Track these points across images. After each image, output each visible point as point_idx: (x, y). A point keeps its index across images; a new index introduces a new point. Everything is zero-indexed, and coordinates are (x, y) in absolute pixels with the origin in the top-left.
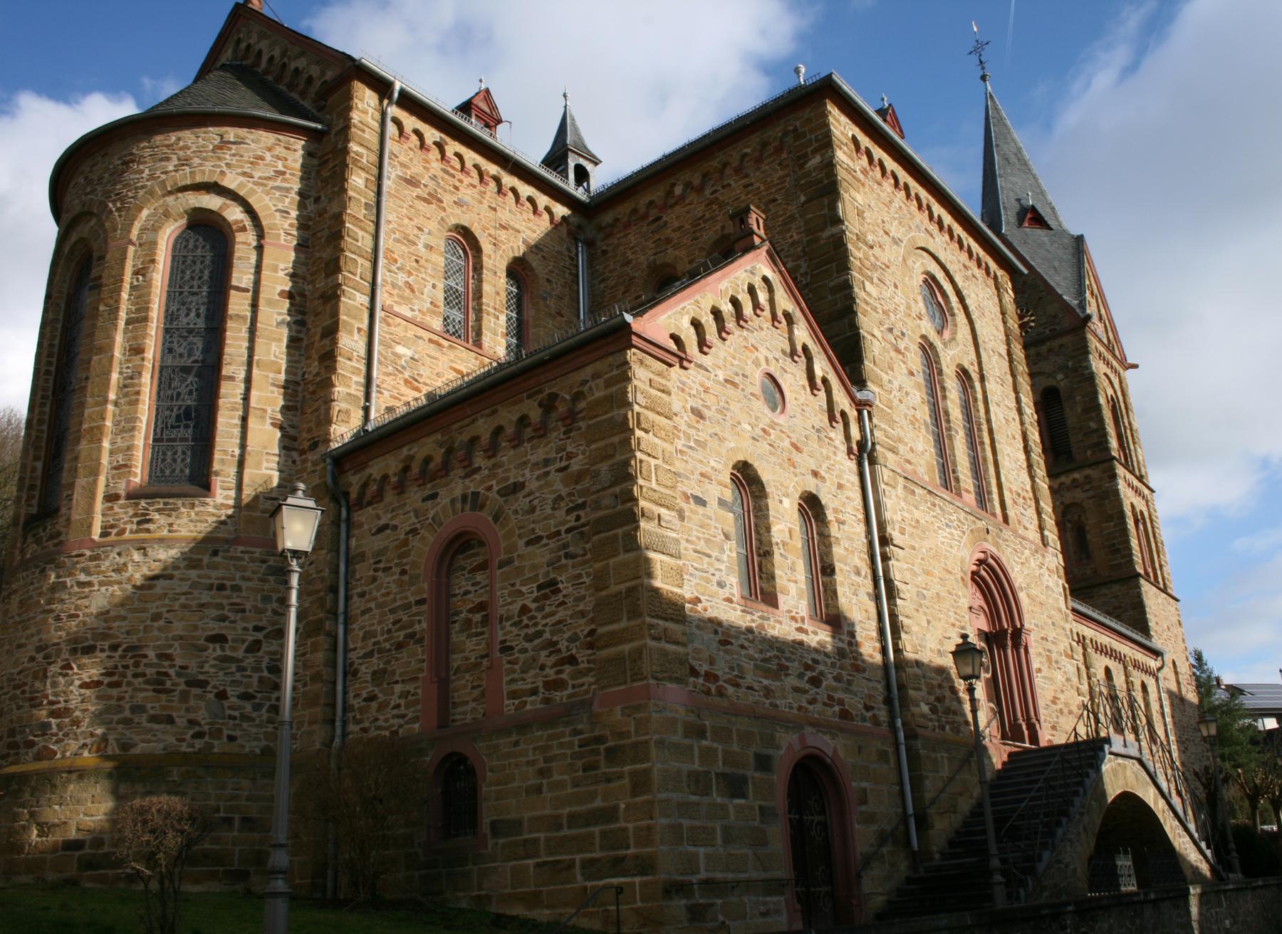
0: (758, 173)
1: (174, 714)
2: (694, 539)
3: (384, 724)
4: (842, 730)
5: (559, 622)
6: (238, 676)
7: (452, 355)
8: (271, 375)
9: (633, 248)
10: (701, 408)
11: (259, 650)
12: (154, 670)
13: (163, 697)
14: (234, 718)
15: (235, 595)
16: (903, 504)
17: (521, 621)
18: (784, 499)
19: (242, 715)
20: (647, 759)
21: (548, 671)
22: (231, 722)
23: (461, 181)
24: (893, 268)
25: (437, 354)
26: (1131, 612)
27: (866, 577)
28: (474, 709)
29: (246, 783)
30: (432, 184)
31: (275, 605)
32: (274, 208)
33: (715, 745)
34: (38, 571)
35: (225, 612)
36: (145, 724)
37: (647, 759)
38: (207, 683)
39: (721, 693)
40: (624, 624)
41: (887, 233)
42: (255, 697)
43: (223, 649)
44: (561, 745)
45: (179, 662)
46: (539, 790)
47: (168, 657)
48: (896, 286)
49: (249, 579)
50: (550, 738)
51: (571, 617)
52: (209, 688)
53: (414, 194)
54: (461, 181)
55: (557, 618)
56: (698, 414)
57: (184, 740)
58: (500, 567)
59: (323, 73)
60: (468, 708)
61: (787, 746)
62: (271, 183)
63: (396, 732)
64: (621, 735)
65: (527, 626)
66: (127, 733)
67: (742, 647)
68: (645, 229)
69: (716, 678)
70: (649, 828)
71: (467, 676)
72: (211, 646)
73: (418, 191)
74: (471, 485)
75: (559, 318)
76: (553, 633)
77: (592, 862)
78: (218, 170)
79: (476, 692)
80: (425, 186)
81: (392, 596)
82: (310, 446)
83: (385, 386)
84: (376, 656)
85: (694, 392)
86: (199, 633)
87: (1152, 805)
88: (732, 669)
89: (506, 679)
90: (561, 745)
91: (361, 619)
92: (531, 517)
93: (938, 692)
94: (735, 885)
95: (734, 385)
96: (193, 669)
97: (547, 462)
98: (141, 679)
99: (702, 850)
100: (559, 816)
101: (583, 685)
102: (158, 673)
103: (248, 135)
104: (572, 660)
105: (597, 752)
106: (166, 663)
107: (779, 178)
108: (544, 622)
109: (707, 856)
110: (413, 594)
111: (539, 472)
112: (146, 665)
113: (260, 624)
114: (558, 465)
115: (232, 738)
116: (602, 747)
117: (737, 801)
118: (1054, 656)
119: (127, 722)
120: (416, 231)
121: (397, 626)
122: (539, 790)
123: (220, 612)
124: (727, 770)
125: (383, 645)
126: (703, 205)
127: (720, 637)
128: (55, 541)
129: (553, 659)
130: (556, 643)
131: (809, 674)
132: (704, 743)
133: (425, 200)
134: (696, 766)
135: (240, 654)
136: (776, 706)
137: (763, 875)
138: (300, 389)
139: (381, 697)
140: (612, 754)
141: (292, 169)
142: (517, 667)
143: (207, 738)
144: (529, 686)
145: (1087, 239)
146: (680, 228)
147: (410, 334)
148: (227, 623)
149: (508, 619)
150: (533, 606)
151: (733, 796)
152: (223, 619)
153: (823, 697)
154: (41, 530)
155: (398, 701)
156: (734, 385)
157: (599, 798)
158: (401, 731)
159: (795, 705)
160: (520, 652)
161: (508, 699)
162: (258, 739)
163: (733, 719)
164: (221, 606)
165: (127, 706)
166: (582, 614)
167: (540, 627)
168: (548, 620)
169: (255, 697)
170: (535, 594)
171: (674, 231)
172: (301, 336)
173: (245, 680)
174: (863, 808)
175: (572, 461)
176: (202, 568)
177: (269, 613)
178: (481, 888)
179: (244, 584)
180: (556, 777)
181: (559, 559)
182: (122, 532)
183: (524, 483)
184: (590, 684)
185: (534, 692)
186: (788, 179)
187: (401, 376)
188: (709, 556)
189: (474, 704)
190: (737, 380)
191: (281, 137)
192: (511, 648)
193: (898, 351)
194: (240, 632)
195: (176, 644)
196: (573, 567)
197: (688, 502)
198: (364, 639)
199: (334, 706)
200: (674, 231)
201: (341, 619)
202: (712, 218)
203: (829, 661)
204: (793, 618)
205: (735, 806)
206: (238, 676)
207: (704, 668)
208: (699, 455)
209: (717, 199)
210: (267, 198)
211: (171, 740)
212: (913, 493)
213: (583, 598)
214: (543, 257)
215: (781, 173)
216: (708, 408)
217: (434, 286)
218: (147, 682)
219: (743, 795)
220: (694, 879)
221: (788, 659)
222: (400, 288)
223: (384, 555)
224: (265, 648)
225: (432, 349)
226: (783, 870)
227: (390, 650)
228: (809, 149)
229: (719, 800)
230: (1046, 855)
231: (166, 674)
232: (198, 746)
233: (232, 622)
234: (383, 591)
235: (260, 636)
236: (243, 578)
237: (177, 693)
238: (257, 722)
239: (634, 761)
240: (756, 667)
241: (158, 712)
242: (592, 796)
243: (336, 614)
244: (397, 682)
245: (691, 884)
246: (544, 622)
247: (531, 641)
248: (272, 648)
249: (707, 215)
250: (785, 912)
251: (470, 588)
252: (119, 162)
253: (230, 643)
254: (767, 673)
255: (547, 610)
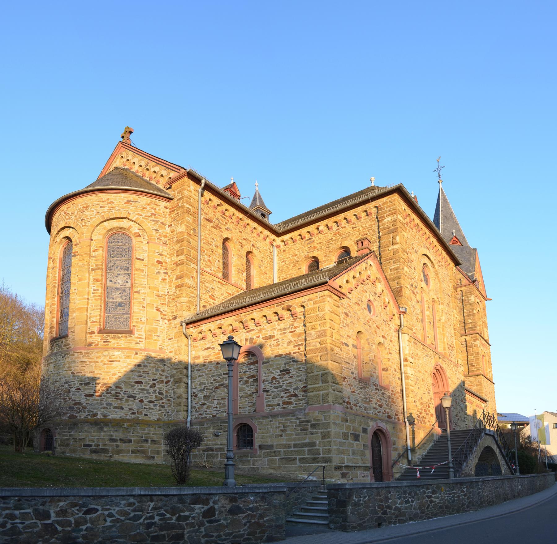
0: (359, 223)
1: (123, 406)
2: (344, 357)
3: (209, 413)
4: (389, 422)
5: (290, 383)
6: (147, 395)
7: (227, 287)
8: (155, 292)
9: (298, 250)
10: (348, 312)
11: (155, 387)
12: (115, 392)
13: (119, 401)
14: (147, 408)
15: (145, 368)
16: (413, 348)
17: (272, 382)
18: (373, 345)
19: (149, 408)
20: (330, 428)
21: (284, 398)
22: (146, 410)
23: (228, 220)
24: (414, 262)
25: (222, 287)
26: (476, 387)
27: (398, 372)
28: (249, 410)
29: (152, 429)
30: (217, 221)
31: (160, 372)
32: (152, 229)
33: (350, 425)
34: (62, 357)
35: (141, 374)
36: (112, 409)
37: (330, 428)
38: (136, 397)
39: (351, 408)
40: (320, 384)
41: (413, 248)
42: (154, 402)
43: (141, 386)
44: (291, 422)
45: (124, 389)
46: (281, 436)
47: (120, 388)
48: (415, 269)
49: (150, 363)
50: (286, 420)
51: (295, 381)
52: (136, 399)
53: (211, 225)
54: (228, 220)
55: (289, 381)
56: (346, 314)
57: (128, 415)
58: (263, 363)
59: (169, 174)
60: (247, 409)
61: (372, 426)
62: (150, 218)
63: (216, 416)
64: (318, 420)
65: (275, 384)
66: (105, 412)
67: (358, 394)
68: (304, 243)
69: (350, 403)
70: (329, 449)
71: (246, 399)
72: (136, 385)
73: (211, 224)
74: (250, 335)
75: (265, 275)
76: (286, 387)
77: (304, 458)
78: (127, 212)
79: (250, 404)
80: (215, 222)
81: (212, 371)
82: (173, 318)
83: (202, 298)
84: (206, 390)
85: (346, 307)
86: (131, 380)
87: (495, 450)
88: (355, 400)
89: (265, 401)
90: (291, 422)
91: (198, 379)
92: (277, 347)
93: (420, 411)
94: (355, 468)
95: (359, 305)
96: (130, 392)
97: (285, 329)
98: (109, 395)
99: (346, 456)
100: (289, 444)
101: (300, 404)
102: (116, 393)
103: (139, 199)
104: (296, 395)
105: (307, 425)
106: (119, 390)
107: (370, 225)
108: (283, 383)
109: (348, 459)
110: (222, 371)
111: (281, 332)
112: (111, 390)
113: (155, 378)
114: (290, 330)
115: (146, 415)
116: (309, 424)
117: (356, 442)
118: (458, 401)
119: (105, 408)
120: (211, 240)
121: (215, 381)
122: (281, 436)
123: (139, 374)
124: (354, 432)
125: (209, 387)
126: (332, 234)
127: (352, 390)
128: (68, 347)
129: (287, 395)
130: (288, 390)
131: (378, 403)
132: (347, 423)
133: (214, 228)
134: (345, 431)
135: (148, 388)
136: (368, 413)
137: (364, 465)
138: (167, 297)
139: (208, 404)
140: (313, 426)
141: (158, 213)
142: (271, 397)
143: (136, 414)
144: (276, 403)
145: (478, 250)
146: (321, 243)
147: (211, 279)
148: (142, 377)
149: (266, 381)
150: (278, 377)
151: (355, 441)
152: (141, 376)
153: (382, 411)
154: (60, 343)
155: (216, 406)
156: (359, 305)
157: (308, 439)
158: (217, 415)
159: (374, 413)
160: (272, 392)
161: (266, 407)
162: (156, 416)
163: (356, 417)
164: (140, 372)
165: (105, 403)
166: (300, 381)
167: (281, 384)
168: (285, 382)
169: (154, 402)
170: (279, 373)
171: (318, 244)
172: (166, 278)
173: (150, 396)
174: (394, 446)
175: (297, 329)
176: (131, 358)
177: (158, 375)
178: (254, 465)
179: (148, 365)
180: (288, 432)
181: (290, 362)
182: (98, 345)
183: (274, 336)
184: (303, 404)
185: (279, 405)
186: (374, 226)
187: (208, 294)
188: (349, 363)
189: (249, 408)
190: (360, 303)
191: (153, 200)
192: (269, 391)
193: (414, 293)
194: (147, 381)
195: (123, 384)
196: (297, 365)
197: (343, 345)
198: (200, 385)
199: (188, 406)
200: (318, 244)
201: (190, 378)
202: (336, 240)
203: (385, 399)
204: (374, 385)
205: (356, 444)
206: (147, 395)
207: (347, 400)
208: (347, 329)
209: (339, 232)
210: (149, 224)
211: (123, 414)
212: (417, 344)
213: (301, 375)
214: (260, 251)
215: (370, 223)
216: (350, 312)
217: (219, 261)
218: (112, 396)
219: (358, 441)
220: (343, 465)
221: (372, 398)
222: (206, 262)
223: (208, 357)
224: (157, 386)
225: (219, 285)
226: (369, 464)
227: (212, 389)
228: (385, 215)
229: (351, 442)
230: (465, 464)
231: (119, 393)
232: (133, 417)
233: (144, 377)
234: (208, 369)
235: (155, 382)
236: (148, 363)
237: (124, 400)
238: (155, 410)
239: (323, 429)
240: (362, 400)
241: (117, 405)
242: (305, 439)
243: (187, 376)
244: (216, 400)
245: (342, 466)
246: (283, 383)
247: (277, 388)
248: (160, 386)
249: (334, 238)
250: (369, 476)
251: (247, 370)
252: (81, 207)
253: (144, 384)
254: (366, 402)
255: (284, 379)
